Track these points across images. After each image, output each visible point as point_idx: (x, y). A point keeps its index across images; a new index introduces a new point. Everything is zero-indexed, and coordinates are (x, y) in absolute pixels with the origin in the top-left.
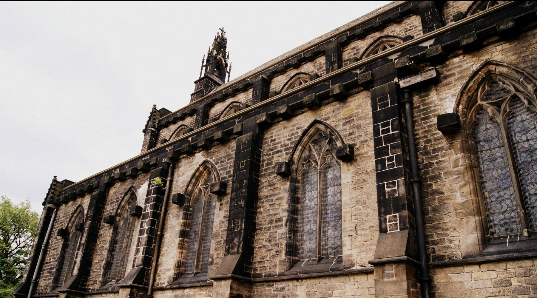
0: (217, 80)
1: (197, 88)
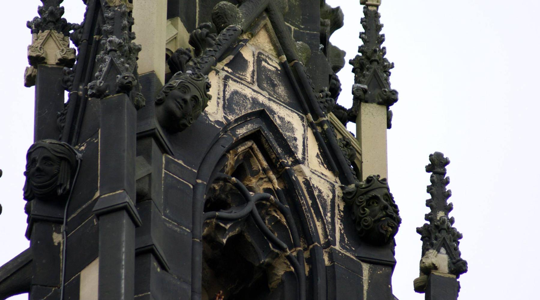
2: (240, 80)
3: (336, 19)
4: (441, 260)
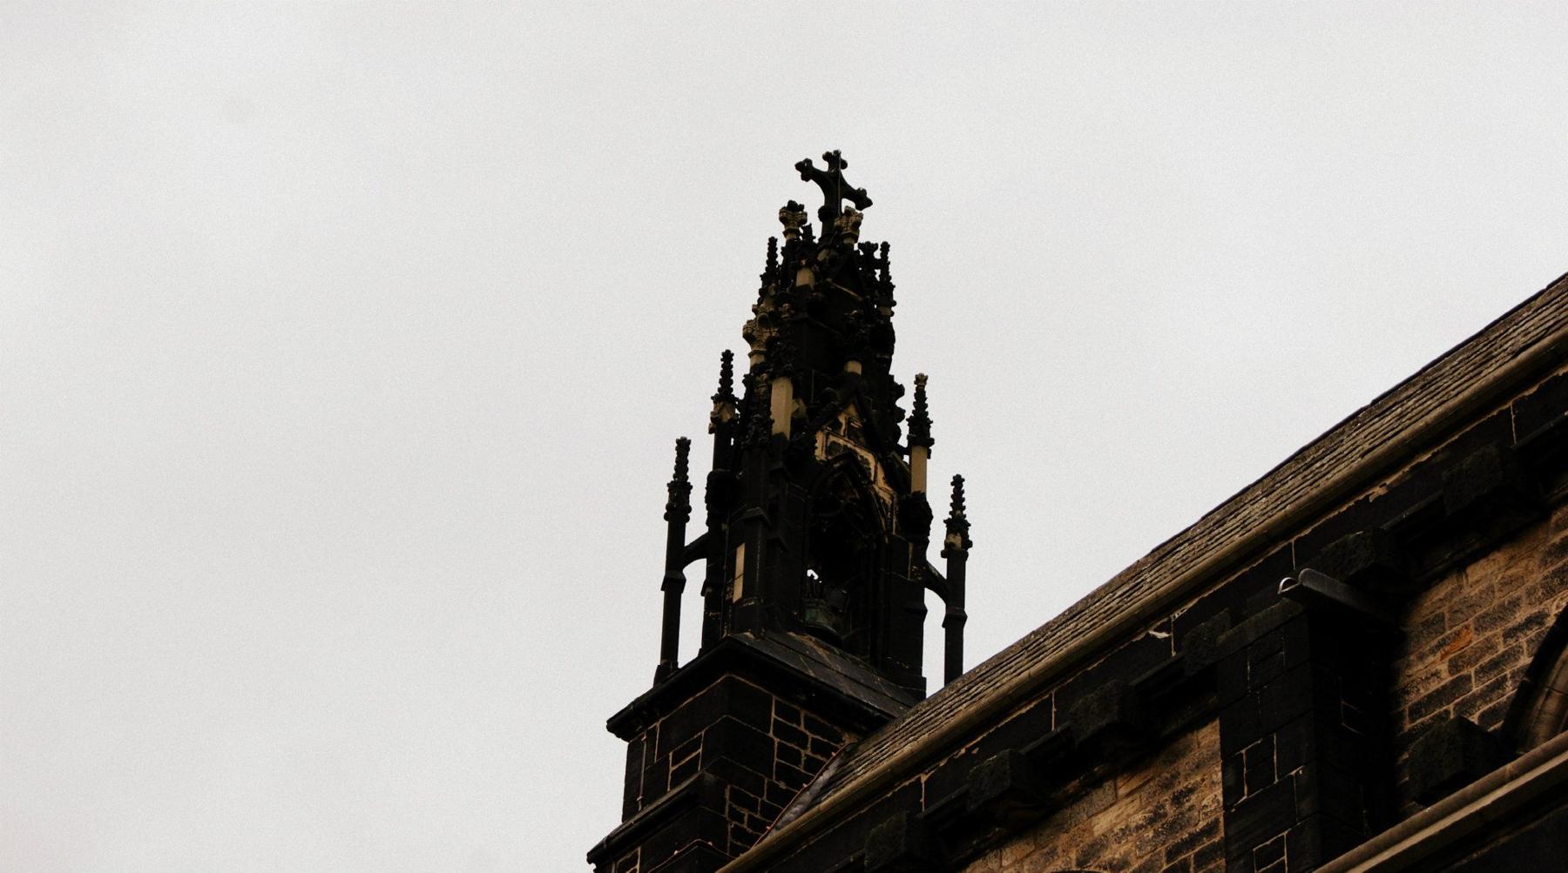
0: (835, 670)
1: (641, 784)
2: (837, 435)
3: (900, 391)
4: (957, 540)
